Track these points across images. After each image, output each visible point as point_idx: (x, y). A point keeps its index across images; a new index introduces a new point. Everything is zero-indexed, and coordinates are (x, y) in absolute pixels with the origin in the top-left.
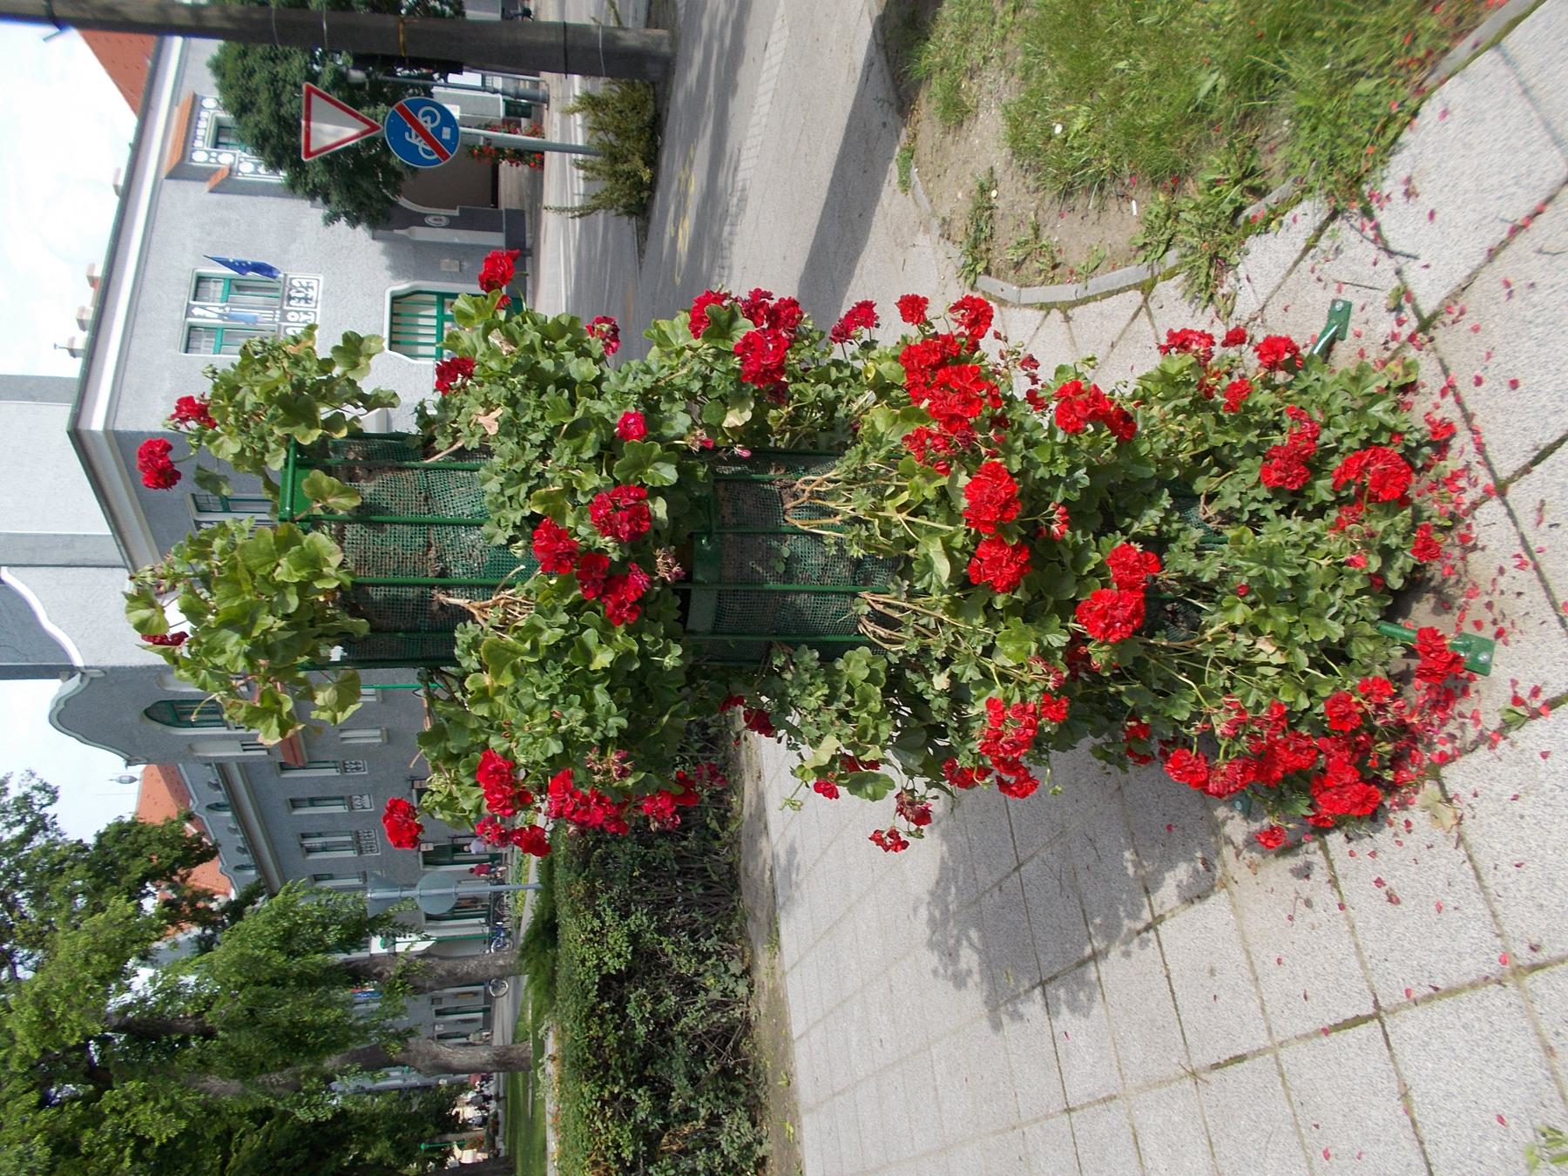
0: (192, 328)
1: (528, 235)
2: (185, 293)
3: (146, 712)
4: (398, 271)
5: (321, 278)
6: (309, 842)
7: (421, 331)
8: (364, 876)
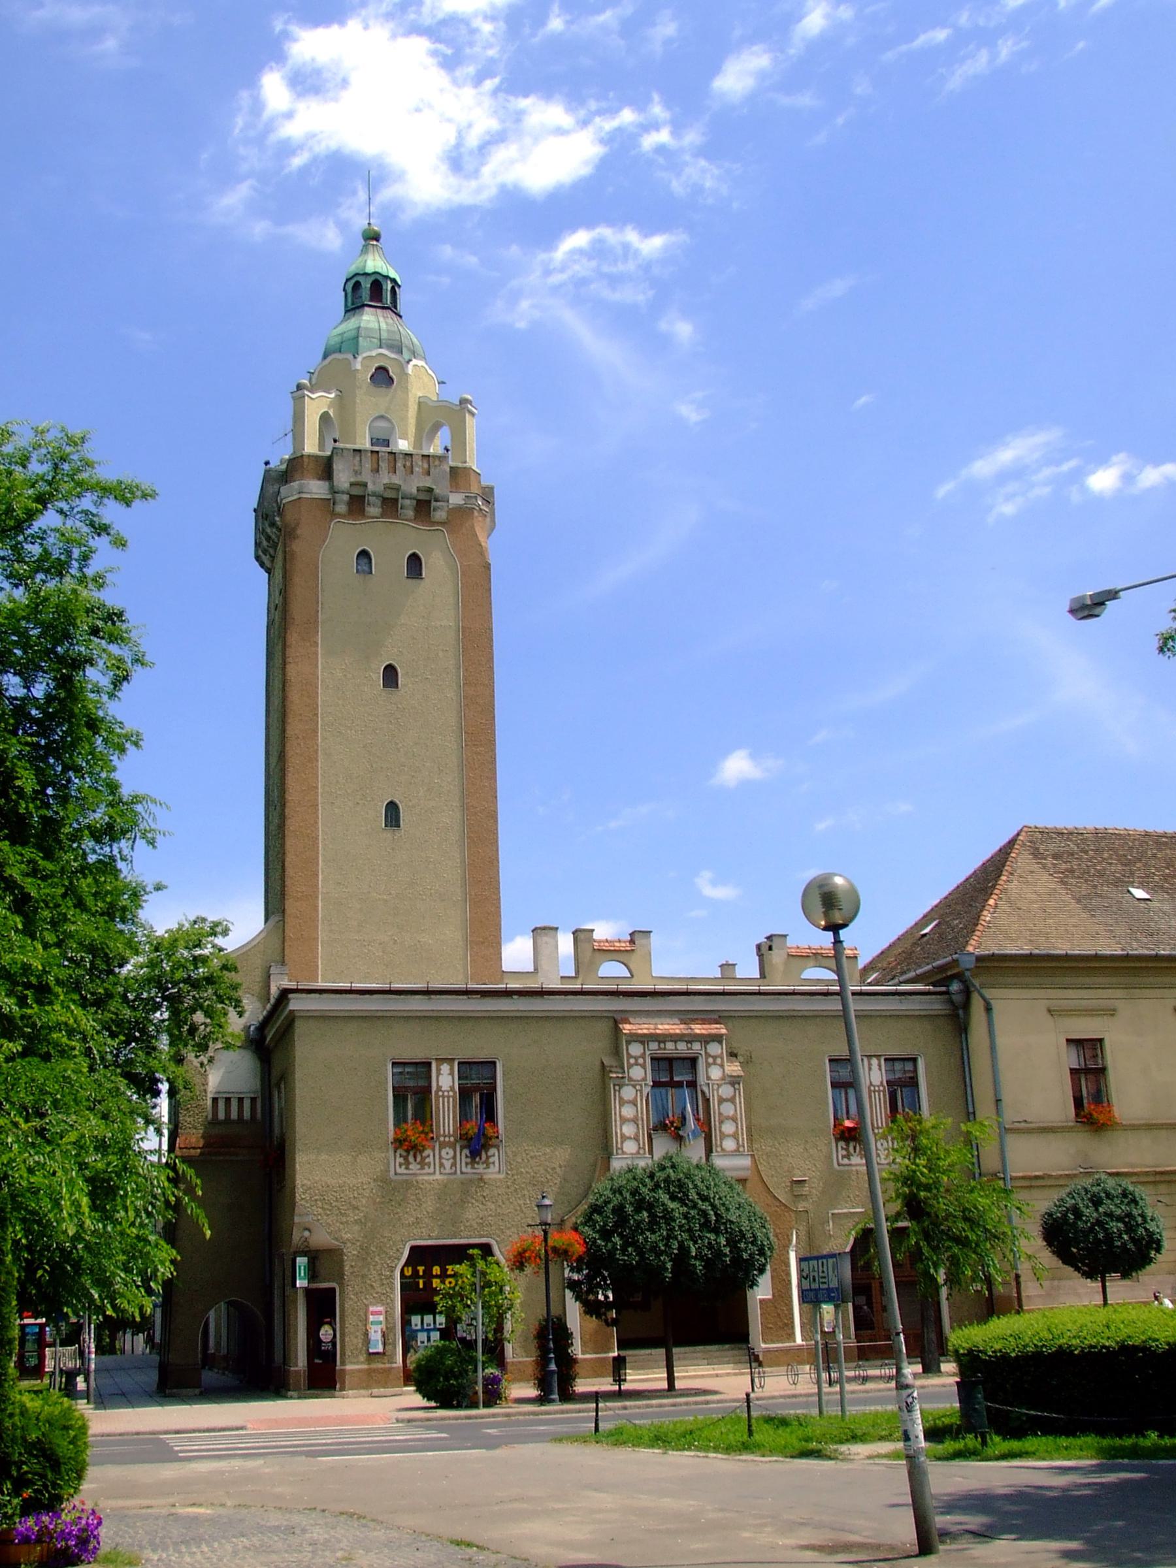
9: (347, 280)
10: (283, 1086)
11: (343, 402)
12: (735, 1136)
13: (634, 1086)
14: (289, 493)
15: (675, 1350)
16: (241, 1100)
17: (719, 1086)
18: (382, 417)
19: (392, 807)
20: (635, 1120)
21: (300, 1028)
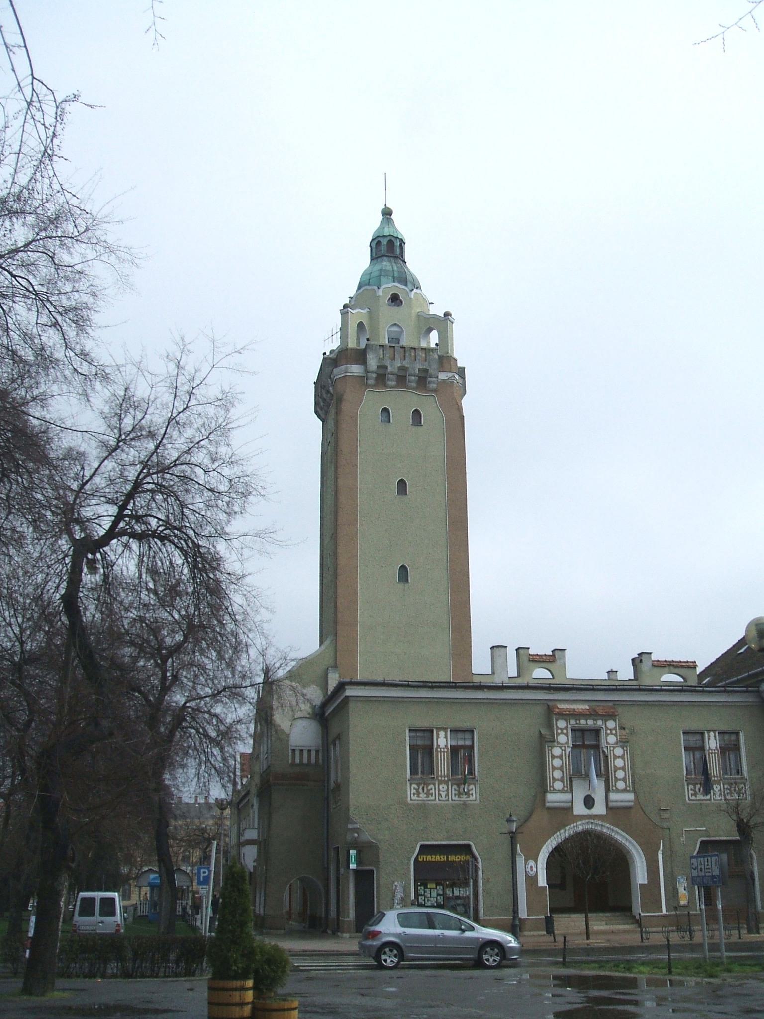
9: (373, 240)
10: (337, 742)
11: (372, 315)
12: (624, 780)
13: (560, 748)
14: (339, 372)
15: (590, 915)
16: (309, 751)
17: (614, 748)
18: (395, 325)
19: (403, 569)
20: (561, 768)
21: (352, 705)
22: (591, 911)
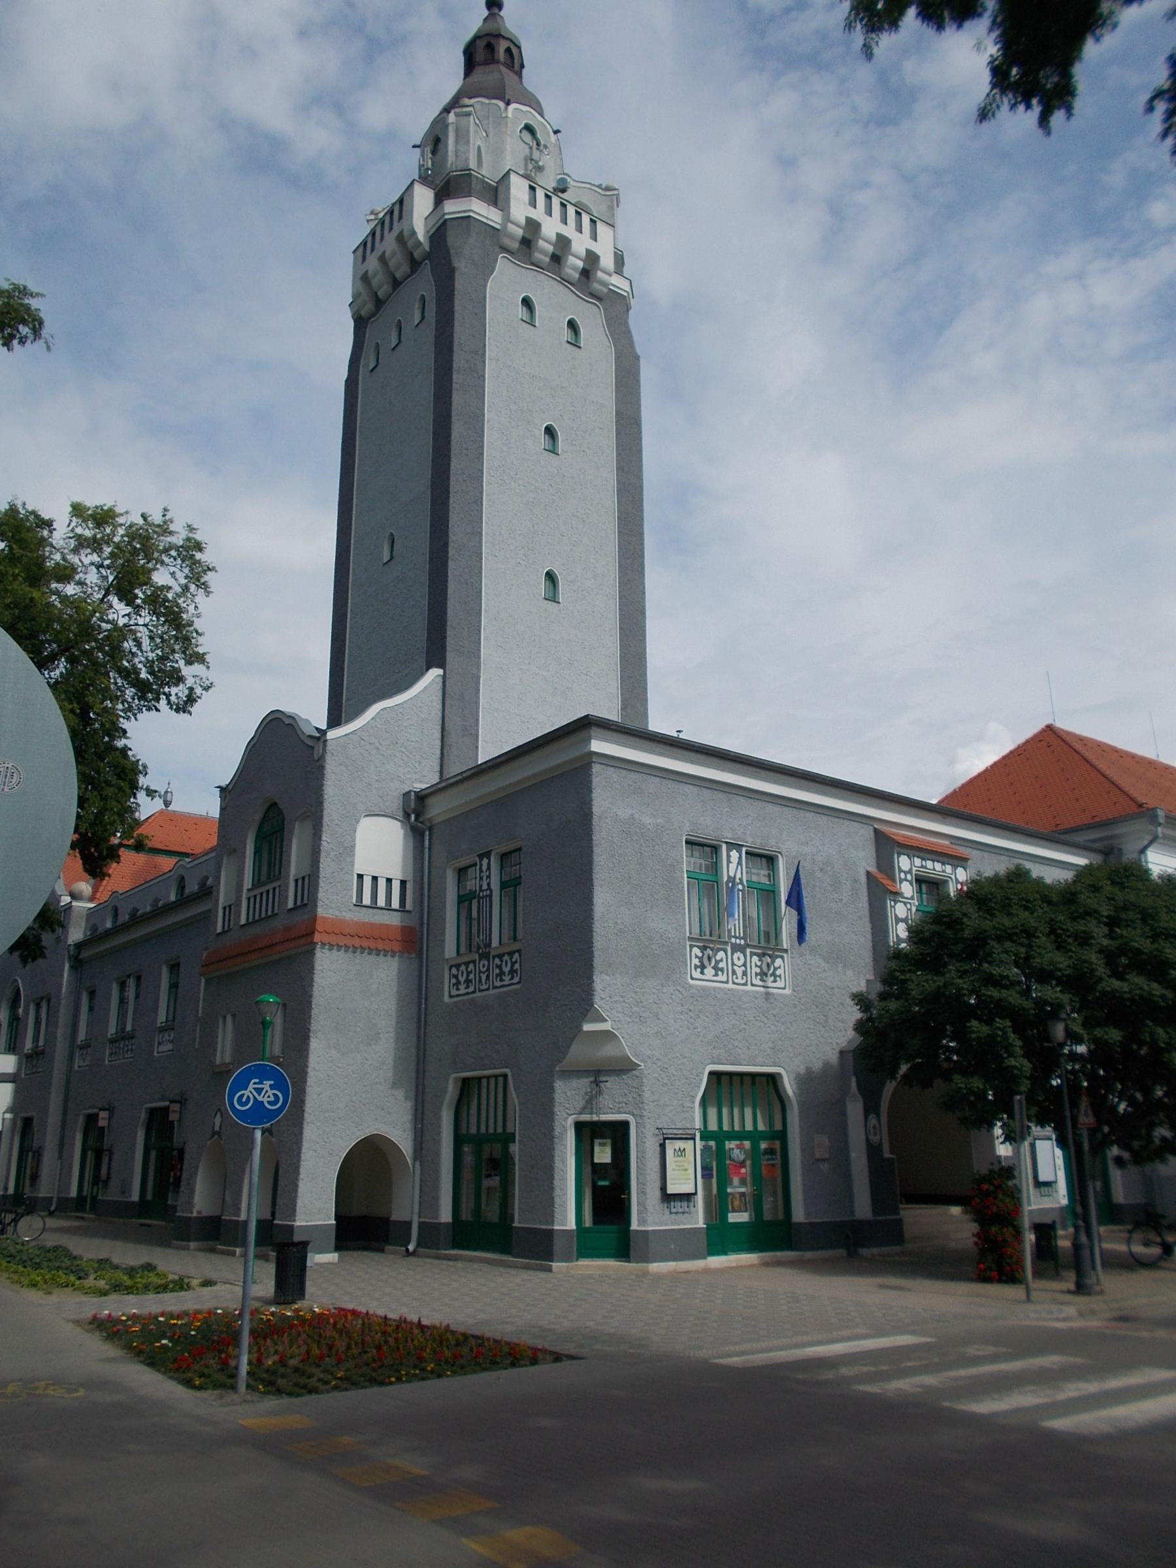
0: (715, 849)
1: (875, 1250)
2: (751, 841)
3: (275, 804)
4: (806, 1081)
5: (787, 991)
6: (131, 983)
7: (736, 1111)
8: (85, 1046)
22: (17, 1093)
